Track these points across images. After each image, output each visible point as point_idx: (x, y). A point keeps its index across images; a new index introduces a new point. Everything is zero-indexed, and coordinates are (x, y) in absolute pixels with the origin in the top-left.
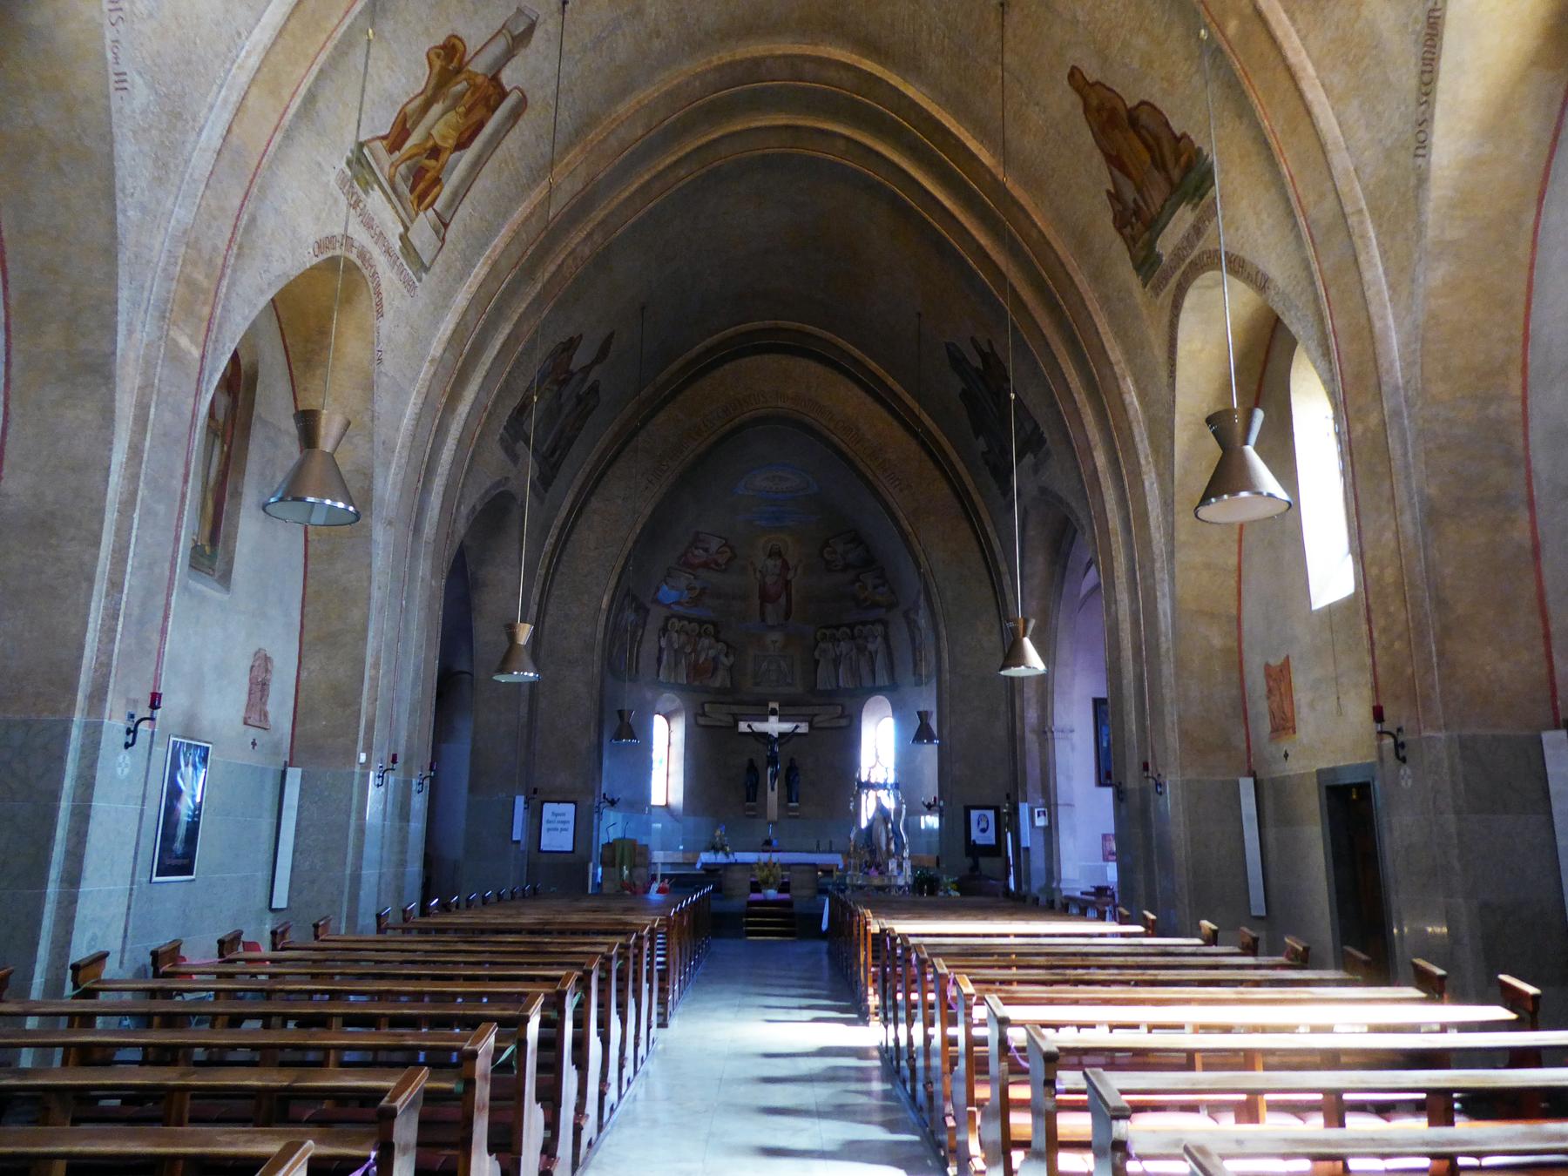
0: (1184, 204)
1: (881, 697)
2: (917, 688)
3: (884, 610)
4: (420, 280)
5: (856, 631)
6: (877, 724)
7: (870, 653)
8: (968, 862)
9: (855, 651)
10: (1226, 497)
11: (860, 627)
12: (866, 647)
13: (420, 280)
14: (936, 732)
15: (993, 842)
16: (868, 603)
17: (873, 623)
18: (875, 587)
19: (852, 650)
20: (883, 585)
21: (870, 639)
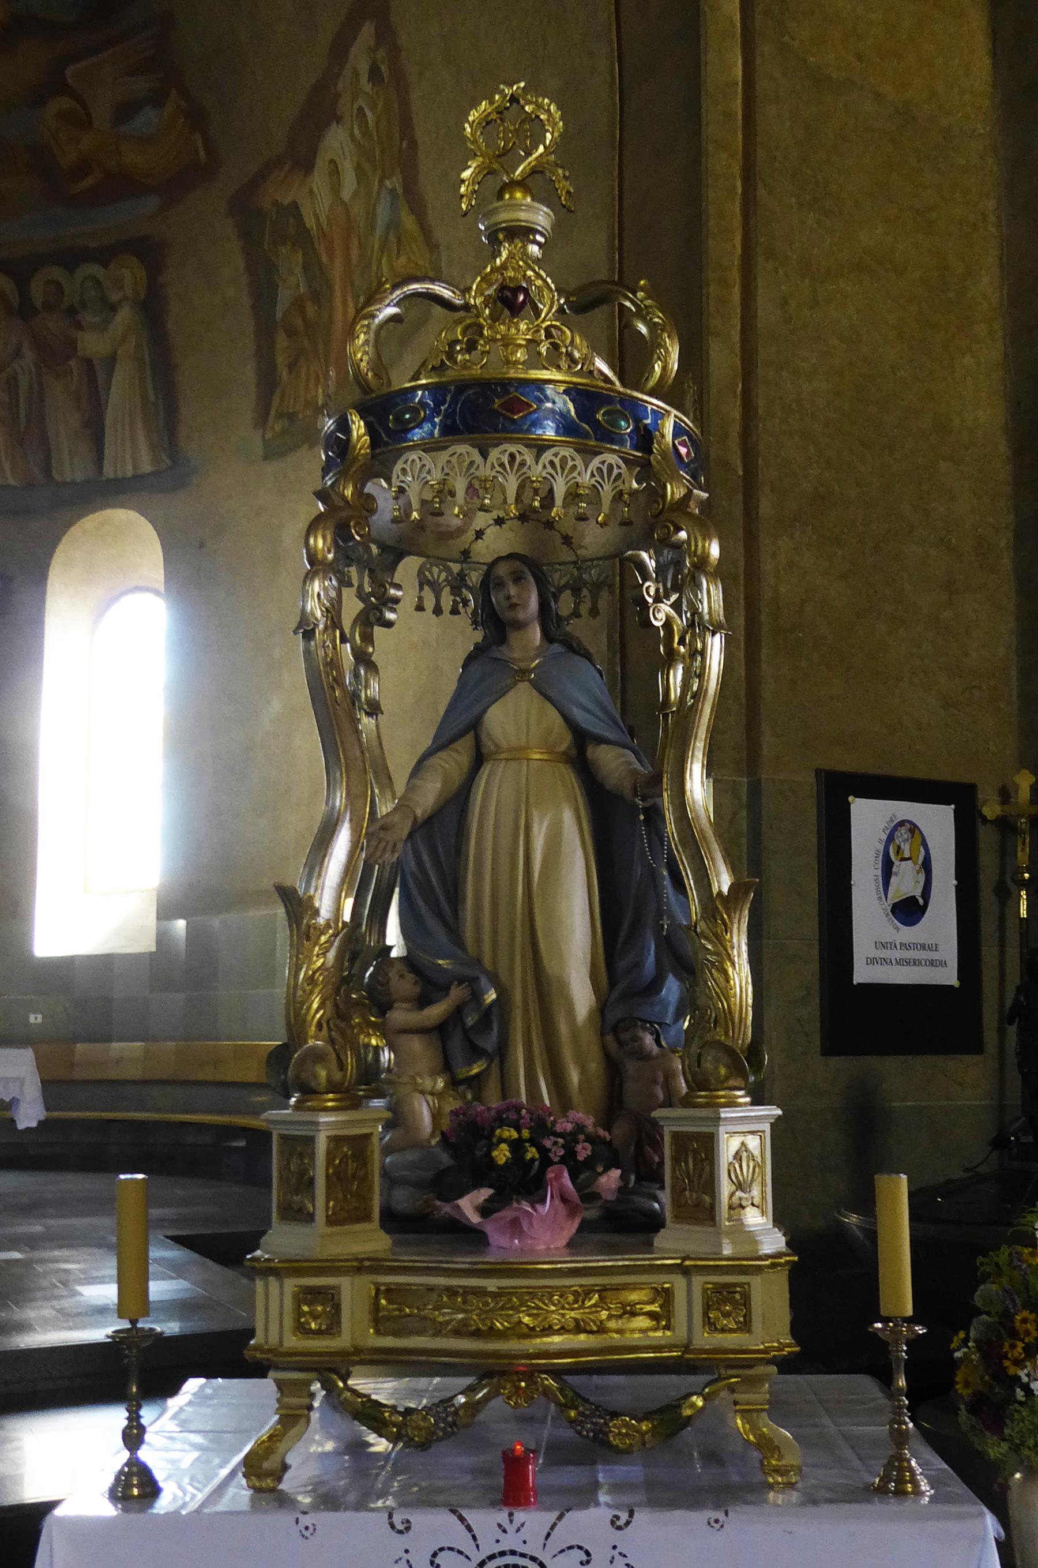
0: (747, 1229)
1: (131, 516)
2: (270, 468)
3: (151, 204)
4: (536, 1210)
5: (37, 289)
6: (100, 612)
7: (89, 362)
8: (253, 1072)
9: (29, 357)
10: (531, 1351)
11: (56, 273)
12: (72, 346)
13: (536, 1210)
14: (348, 636)
15: (949, 976)
16: (88, 182)
17: (105, 256)
18: (124, 112)
19: (18, 354)
20: (157, 99)
21: (88, 318)
